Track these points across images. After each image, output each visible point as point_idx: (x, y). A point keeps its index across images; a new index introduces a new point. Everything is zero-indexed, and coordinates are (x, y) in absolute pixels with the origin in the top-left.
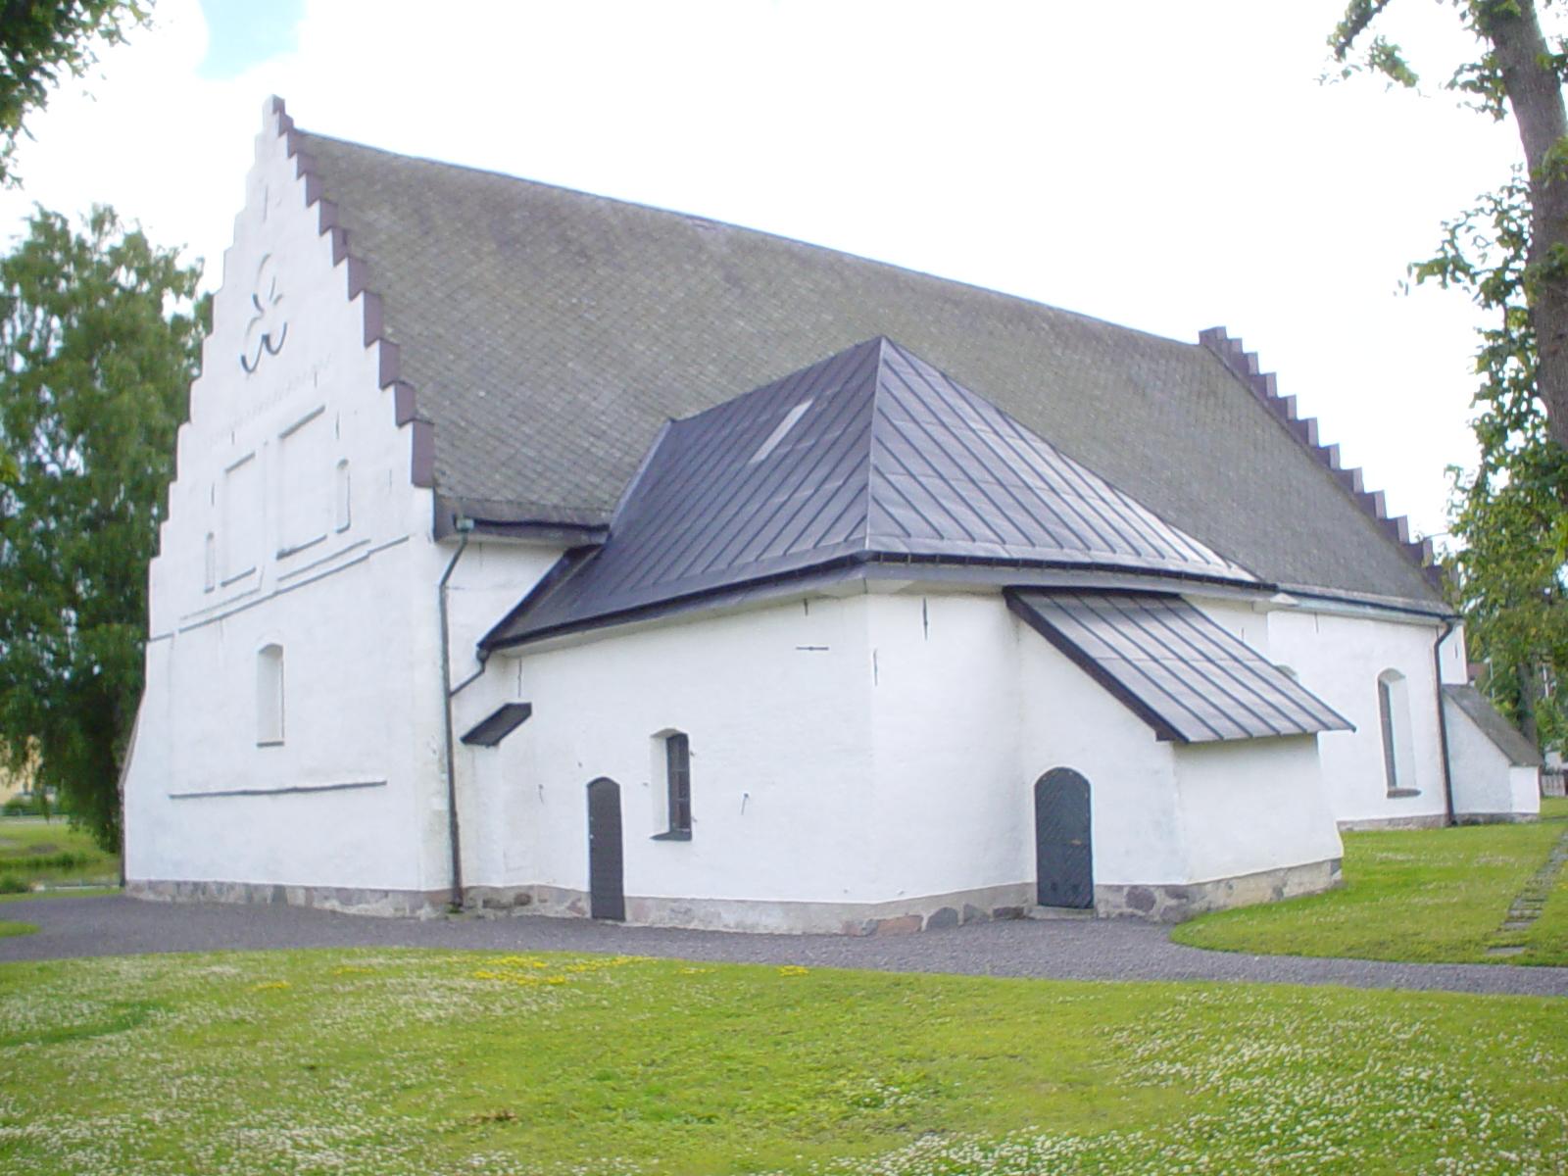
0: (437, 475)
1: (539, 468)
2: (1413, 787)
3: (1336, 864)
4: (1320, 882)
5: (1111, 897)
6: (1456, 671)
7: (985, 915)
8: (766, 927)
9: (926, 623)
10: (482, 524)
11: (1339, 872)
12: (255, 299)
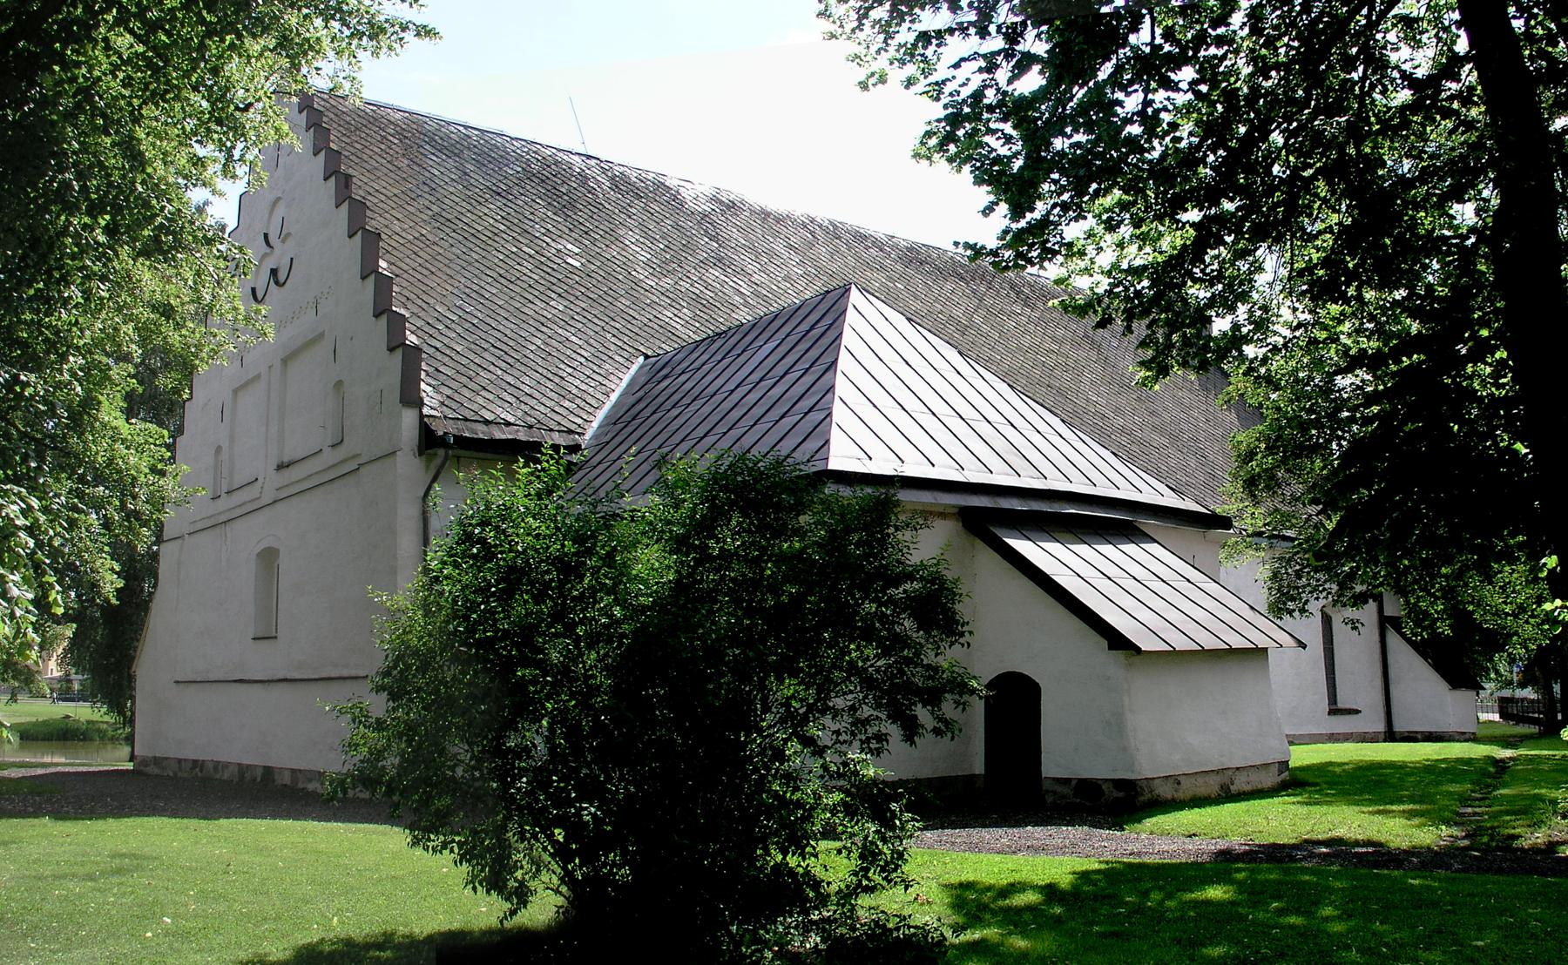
5: (1059, 789)
12: (266, 236)
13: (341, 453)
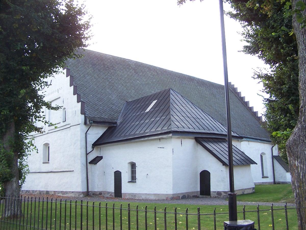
0: (85, 112)
1: (103, 111)
2: (267, 176)
3: (253, 188)
4: (251, 191)
6: (276, 153)
7: (191, 197)
8: (151, 199)
9: (182, 144)
10: (95, 122)
11: (254, 190)
13: (65, 123)
